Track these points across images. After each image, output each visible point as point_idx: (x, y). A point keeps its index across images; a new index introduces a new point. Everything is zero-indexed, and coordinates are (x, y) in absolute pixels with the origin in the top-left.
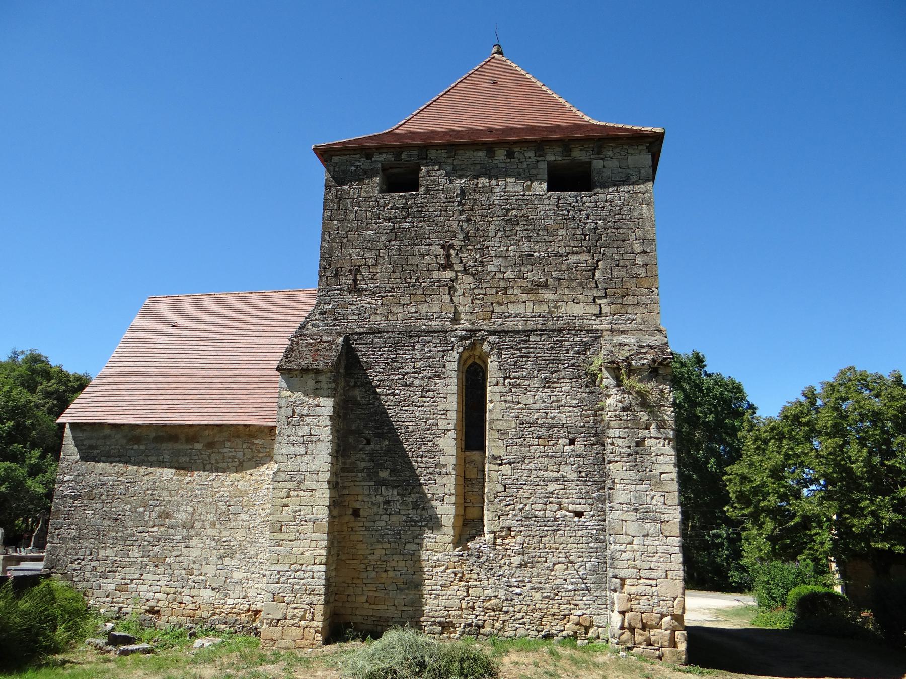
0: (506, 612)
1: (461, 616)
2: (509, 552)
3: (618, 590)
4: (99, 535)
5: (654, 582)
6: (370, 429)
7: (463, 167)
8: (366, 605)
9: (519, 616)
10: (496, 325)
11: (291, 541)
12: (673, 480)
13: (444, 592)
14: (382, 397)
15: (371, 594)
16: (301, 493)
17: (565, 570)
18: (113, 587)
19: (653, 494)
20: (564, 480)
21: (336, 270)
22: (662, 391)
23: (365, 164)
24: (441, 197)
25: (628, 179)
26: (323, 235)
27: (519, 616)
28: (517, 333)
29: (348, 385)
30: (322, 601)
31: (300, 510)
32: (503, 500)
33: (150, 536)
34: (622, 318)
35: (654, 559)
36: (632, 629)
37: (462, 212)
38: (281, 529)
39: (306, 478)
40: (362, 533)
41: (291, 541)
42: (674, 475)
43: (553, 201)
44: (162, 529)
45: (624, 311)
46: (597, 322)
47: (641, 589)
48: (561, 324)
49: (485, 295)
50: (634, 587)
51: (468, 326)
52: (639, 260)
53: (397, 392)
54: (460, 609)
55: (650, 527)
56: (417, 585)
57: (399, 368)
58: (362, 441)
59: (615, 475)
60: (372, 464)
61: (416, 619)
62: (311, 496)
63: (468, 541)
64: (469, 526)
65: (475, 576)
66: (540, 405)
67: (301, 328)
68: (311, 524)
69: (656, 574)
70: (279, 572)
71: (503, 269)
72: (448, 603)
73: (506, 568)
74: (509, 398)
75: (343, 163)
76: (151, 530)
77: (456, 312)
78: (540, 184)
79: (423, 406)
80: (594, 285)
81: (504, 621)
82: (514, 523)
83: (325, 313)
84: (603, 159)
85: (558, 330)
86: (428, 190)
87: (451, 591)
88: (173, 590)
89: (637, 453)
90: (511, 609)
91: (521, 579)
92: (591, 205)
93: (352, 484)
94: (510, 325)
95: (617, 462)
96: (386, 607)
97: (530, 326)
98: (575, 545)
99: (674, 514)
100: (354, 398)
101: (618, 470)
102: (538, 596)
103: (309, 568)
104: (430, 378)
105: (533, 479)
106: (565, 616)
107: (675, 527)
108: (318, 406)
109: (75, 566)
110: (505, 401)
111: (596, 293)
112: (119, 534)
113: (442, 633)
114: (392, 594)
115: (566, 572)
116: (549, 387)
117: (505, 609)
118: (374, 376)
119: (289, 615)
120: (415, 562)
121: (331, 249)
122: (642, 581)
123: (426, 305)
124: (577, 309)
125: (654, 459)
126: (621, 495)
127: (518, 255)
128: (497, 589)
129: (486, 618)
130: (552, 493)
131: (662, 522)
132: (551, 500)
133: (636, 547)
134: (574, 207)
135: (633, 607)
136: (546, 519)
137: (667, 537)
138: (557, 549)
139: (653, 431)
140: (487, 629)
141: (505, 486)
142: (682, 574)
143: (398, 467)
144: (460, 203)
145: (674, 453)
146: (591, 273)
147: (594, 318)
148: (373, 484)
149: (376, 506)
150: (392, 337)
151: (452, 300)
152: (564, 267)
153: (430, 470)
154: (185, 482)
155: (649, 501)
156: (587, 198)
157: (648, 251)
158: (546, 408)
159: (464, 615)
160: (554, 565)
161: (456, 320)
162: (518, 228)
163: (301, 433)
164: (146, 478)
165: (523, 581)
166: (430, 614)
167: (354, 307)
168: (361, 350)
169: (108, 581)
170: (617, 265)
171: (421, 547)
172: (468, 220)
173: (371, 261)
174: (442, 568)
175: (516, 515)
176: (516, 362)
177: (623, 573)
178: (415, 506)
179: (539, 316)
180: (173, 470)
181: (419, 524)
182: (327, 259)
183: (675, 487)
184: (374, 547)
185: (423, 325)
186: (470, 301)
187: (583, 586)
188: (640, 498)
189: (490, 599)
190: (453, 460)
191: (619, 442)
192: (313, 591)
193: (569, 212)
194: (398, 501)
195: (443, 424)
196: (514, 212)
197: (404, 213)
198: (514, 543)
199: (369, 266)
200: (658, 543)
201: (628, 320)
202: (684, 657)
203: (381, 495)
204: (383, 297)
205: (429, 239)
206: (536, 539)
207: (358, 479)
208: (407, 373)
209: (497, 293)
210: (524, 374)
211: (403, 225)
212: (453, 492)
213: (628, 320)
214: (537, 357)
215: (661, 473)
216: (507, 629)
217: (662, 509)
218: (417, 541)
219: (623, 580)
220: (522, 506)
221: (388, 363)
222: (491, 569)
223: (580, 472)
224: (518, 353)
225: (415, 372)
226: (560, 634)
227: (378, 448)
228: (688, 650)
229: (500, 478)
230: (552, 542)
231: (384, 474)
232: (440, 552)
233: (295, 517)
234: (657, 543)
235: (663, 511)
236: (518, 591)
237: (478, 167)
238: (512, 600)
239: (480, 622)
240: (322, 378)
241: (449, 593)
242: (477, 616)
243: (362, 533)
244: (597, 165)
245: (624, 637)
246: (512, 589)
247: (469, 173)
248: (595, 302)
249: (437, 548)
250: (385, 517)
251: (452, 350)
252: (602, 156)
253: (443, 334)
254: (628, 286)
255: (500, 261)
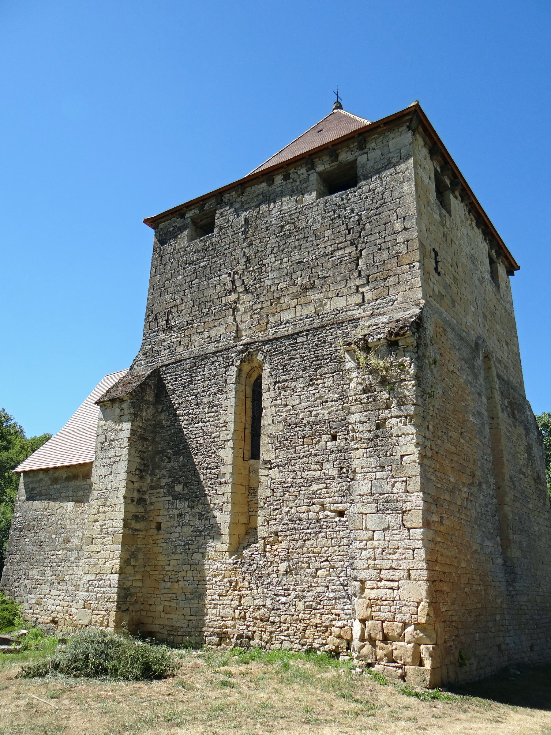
0: (273, 623)
1: (234, 626)
2: (277, 559)
3: (358, 594)
4: (31, 558)
5: (395, 585)
6: (171, 449)
7: (249, 201)
8: (163, 615)
9: (284, 627)
10: (270, 334)
11: (98, 552)
12: (414, 461)
13: (221, 602)
14: (180, 418)
15: (166, 603)
16: (106, 509)
17: (327, 576)
18: (34, 601)
19: (393, 480)
20: (325, 479)
21: (156, 315)
22: (402, 364)
23: (179, 222)
24: (230, 232)
25: (389, 162)
26: (150, 289)
27: (284, 627)
28: (286, 337)
29: (157, 412)
30: (114, 609)
31: (105, 524)
32: (271, 505)
33: (58, 558)
34: (385, 301)
35: (395, 557)
36: (372, 641)
37: (244, 240)
38: (92, 542)
39: (111, 495)
40: (162, 545)
41: (98, 552)
42: (416, 457)
43: (321, 206)
44: (65, 552)
45: (385, 293)
46: (360, 310)
47: (382, 592)
48: (326, 321)
49: (262, 308)
50: (375, 591)
51: (248, 340)
52: (400, 239)
53: (191, 411)
54: (234, 619)
55: (392, 519)
56: (200, 595)
57: (193, 389)
58: (164, 460)
59: (356, 464)
60: (171, 480)
61: (198, 629)
62: (113, 511)
63: (244, 549)
64: (245, 534)
65: (246, 585)
66: (305, 404)
67: (130, 369)
68: (111, 536)
69: (397, 575)
70: (89, 581)
71: (277, 281)
72: (224, 613)
73: (274, 575)
74: (278, 402)
75: (164, 226)
76: (58, 553)
77: (238, 330)
78: (311, 194)
79: (209, 421)
80: (356, 275)
81: (271, 633)
82: (280, 528)
83: (147, 352)
84: (367, 153)
85: (322, 327)
86: (221, 229)
87: (227, 600)
88: (66, 604)
89: (377, 436)
90: (277, 619)
91: (286, 587)
92: (355, 199)
93: (156, 500)
94: (282, 332)
95: (358, 449)
96: (176, 616)
97: (299, 328)
98: (336, 548)
99: (416, 502)
100: (160, 422)
101: (360, 459)
102: (301, 605)
103: (108, 577)
104: (215, 394)
105: (298, 480)
106: (327, 627)
107: (416, 518)
108: (121, 430)
109: (17, 584)
110: (275, 406)
111: (358, 282)
112: (41, 558)
113: (219, 644)
114: (182, 604)
115: (328, 578)
116: (313, 384)
117: (271, 619)
118: (176, 400)
119: (93, 620)
120: (199, 572)
121: (153, 299)
122: (383, 582)
123: (215, 329)
124: (340, 303)
125: (394, 441)
126: (361, 487)
127: (290, 264)
128: (265, 598)
129: (255, 628)
130: (314, 494)
131: (404, 512)
132: (314, 500)
133: (376, 543)
134: (339, 206)
135: (374, 614)
136: (309, 521)
137: (409, 529)
138: (320, 553)
139: (395, 411)
140: (256, 642)
141: (273, 490)
142: (425, 573)
143: (190, 481)
144: (244, 232)
145: (415, 431)
146: (354, 265)
147: (357, 307)
148: (171, 498)
149: (172, 520)
150: (186, 365)
151: (235, 319)
152: (330, 265)
153: (212, 481)
154: (80, 512)
155: (389, 489)
156: (350, 194)
157: (409, 226)
158: (310, 406)
159: (237, 626)
160: (317, 570)
161: (237, 337)
162: (290, 240)
163: (109, 456)
164: (59, 511)
165: (288, 589)
166: (210, 624)
167: (165, 343)
168: (167, 378)
169: (32, 596)
170: (379, 249)
171: (204, 557)
172: (250, 245)
173: (178, 302)
174: (221, 577)
175: (282, 519)
176: (285, 366)
177: (362, 574)
178: (201, 517)
179: (306, 318)
180: (73, 503)
181: (203, 533)
182: (150, 309)
183: (416, 470)
184: (170, 558)
185: (212, 348)
186: (249, 317)
187: (344, 594)
188: (380, 486)
189: (259, 609)
190: (229, 469)
191: (360, 427)
192: (109, 599)
193: (334, 212)
194: (188, 513)
195: (223, 436)
196: (287, 227)
197: (203, 254)
198: (280, 548)
199: (177, 306)
200: (399, 537)
201: (390, 301)
202: (428, 678)
203: (176, 508)
204: (185, 330)
205: (220, 270)
206: (300, 543)
207: (161, 495)
208: (198, 393)
209: (271, 304)
210: (291, 375)
211: (202, 264)
212: (230, 500)
213: (390, 301)
214: (303, 357)
215: (403, 456)
216: (274, 642)
217: (403, 497)
218: (201, 550)
219: (362, 582)
220: (287, 509)
221: (185, 387)
222: (261, 577)
223: (342, 468)
224: (286, 357)
225: (204, 391)
226: (322, 649)
227: (175, 465)
228: (433, 669)
229: (269, 482)
230: (314, 546)
231: (179, 488)
232: (219, 560)
233: (101, 531)
234: (397, 537)
235: (405, 499)
236: (283, 599)
237: (261, 197)
238: (278, 609)
239: (250, 634)
240: (125, 406)
241: (225, 603)
242: (248, 626)
243: (162, 545)
244: (362, 159)
245: (365, 651)
246: (278, 598)
247: (253, 204)
248: (358, 291)
249: (217, 556)
250: (178, 529)
251: (232, 364)
252: (365, 151)
253: (225, 352)
254: (389, 267)
255: (275, 274)
